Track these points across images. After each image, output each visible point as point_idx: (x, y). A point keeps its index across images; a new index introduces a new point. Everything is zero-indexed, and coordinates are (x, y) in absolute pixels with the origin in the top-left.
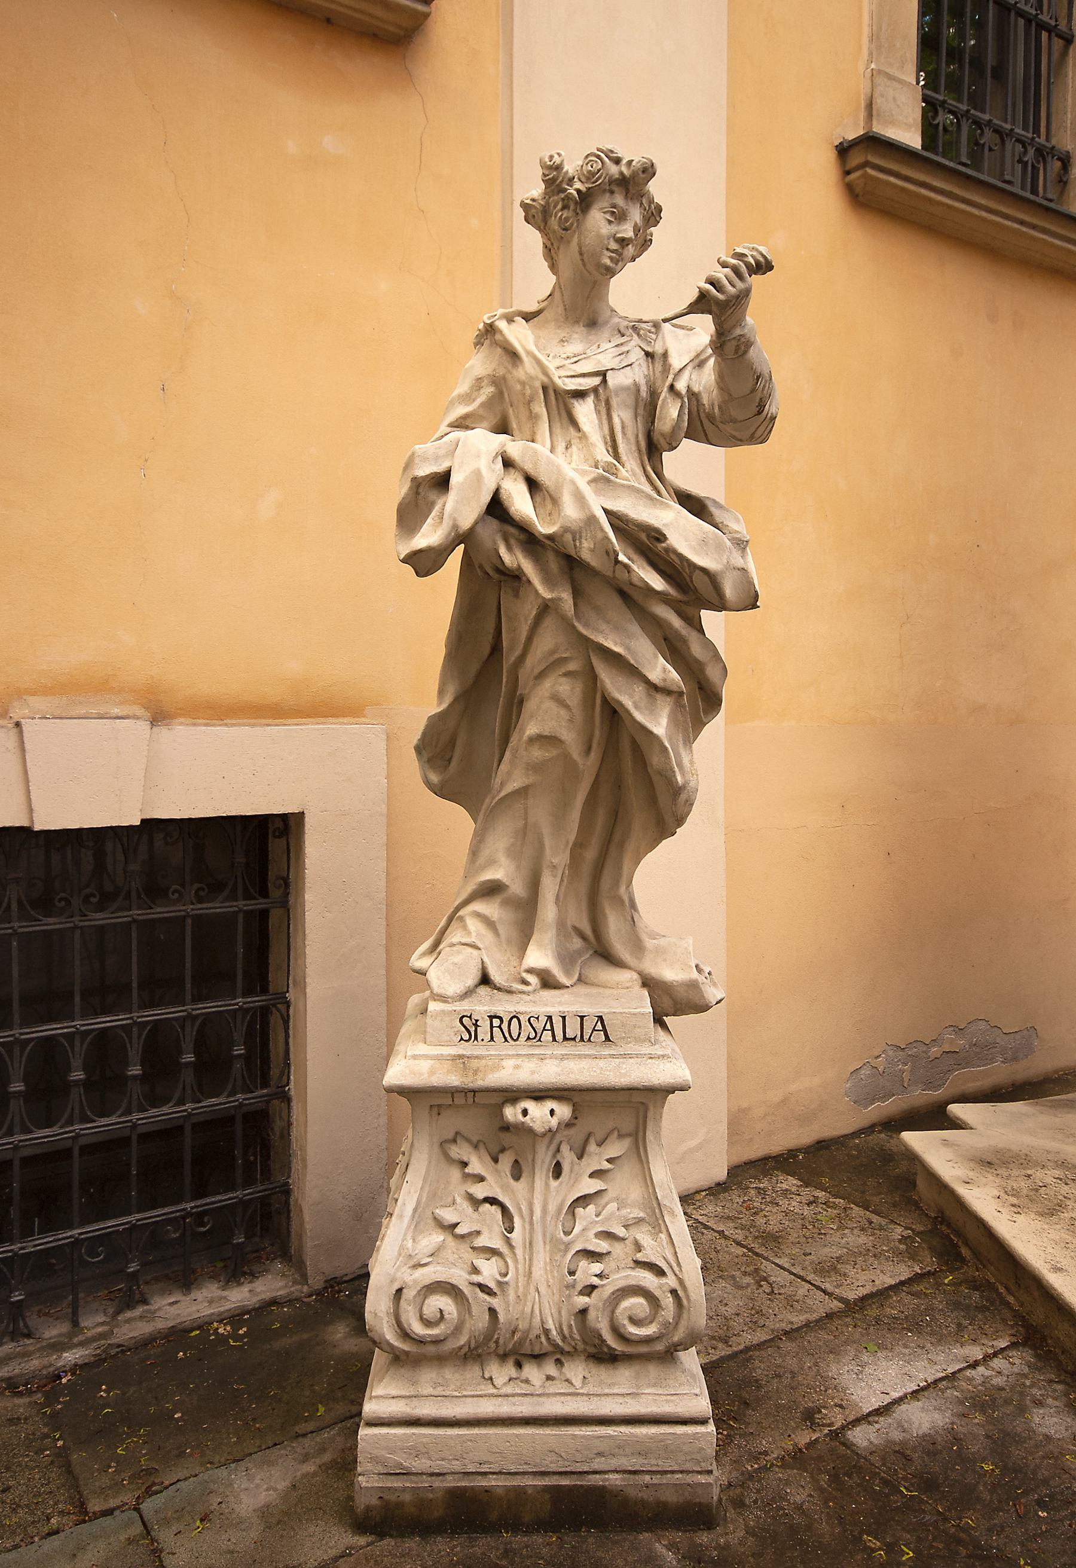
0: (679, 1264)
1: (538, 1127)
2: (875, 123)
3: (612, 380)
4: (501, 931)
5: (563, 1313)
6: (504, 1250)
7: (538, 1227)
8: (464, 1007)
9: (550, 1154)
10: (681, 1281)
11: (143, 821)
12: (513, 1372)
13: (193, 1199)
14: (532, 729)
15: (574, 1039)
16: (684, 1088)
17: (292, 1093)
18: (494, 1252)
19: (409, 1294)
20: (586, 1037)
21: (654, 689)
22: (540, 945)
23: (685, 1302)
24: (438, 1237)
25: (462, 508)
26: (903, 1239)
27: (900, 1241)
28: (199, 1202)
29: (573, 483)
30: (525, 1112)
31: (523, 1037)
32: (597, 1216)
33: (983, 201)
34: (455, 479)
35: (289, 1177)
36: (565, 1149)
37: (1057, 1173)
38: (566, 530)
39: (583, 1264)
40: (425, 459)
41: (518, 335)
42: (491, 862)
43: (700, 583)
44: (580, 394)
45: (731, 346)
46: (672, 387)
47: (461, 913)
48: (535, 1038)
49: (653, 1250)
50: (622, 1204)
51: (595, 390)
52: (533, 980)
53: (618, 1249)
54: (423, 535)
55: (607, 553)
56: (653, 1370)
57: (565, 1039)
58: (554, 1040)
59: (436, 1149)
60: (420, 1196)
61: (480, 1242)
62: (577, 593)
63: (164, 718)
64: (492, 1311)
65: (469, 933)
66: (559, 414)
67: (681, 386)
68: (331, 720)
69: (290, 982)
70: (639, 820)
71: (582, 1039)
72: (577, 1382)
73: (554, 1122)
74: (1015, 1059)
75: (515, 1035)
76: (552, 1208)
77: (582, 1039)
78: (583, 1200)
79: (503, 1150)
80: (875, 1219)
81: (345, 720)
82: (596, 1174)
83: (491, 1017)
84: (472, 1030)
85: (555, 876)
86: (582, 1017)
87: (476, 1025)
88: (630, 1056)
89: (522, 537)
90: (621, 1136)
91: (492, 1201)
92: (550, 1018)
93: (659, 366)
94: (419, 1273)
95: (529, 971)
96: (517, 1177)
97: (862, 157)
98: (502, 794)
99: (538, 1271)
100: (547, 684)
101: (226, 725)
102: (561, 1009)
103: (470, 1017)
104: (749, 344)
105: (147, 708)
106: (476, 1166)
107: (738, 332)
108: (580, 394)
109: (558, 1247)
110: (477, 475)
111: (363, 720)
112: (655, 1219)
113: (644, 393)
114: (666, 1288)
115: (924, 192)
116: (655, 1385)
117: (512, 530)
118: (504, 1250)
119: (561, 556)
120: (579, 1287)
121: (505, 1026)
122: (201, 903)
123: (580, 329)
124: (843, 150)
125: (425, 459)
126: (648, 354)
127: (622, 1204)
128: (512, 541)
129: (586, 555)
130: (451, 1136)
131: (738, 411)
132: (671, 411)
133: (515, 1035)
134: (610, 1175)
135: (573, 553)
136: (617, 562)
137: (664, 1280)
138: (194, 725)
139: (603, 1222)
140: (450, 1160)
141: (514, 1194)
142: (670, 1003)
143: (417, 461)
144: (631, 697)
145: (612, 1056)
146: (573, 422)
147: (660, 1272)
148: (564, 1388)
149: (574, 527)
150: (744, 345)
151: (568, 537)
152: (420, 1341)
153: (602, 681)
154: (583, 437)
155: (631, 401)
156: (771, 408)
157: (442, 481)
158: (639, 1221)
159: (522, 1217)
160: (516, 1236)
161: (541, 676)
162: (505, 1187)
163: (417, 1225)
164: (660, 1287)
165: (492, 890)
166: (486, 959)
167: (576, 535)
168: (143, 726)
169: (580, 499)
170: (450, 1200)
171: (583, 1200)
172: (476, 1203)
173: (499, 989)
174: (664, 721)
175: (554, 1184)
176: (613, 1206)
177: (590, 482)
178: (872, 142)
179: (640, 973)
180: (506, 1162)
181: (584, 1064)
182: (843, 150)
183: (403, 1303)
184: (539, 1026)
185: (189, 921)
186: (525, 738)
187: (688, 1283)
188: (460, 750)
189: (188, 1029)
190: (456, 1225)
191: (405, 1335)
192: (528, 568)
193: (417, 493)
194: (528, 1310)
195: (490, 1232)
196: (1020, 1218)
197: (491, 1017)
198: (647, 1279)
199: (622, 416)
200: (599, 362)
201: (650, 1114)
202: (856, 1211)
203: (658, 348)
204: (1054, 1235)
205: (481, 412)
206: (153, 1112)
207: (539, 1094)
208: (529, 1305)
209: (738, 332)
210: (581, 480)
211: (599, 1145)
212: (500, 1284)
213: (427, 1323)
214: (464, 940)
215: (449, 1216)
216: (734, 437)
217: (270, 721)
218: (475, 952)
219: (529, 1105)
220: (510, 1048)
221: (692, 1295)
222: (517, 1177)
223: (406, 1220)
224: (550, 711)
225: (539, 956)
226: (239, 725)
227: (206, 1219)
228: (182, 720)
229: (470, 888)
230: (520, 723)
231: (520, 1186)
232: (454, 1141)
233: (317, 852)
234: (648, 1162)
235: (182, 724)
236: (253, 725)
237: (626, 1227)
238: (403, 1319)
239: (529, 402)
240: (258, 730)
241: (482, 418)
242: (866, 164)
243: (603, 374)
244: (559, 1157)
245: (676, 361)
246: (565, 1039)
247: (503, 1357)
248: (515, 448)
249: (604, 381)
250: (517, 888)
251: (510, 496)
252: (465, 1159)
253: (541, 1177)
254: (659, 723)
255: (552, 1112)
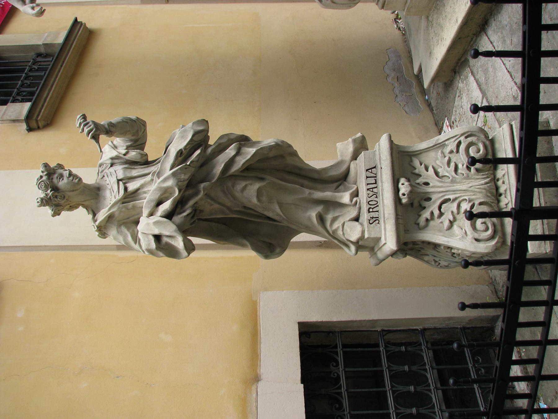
0: (456, 136)
1: (409, 189)
2: (21, 119)
3: (121, 176)
4: (337, 215)
5: (478, 177)
6: (457, 201)
7: (448, 189)
8: (366, 223)
9: (420, 187)
10: (462, 135)
11: (302, 383)
12: (503, 196)
13: (468, 364)
14: (255, 200)
15: (376, 180)
16: (390, 137)
17: (421, 327)
18: (459, 206)
19: (477, 236)
20: (375, 175)
21: (238, 153)
22: (341, 197)
23: (469, 133)
24: (455, 227)
25: (168, 229)
26: (463, 82)
27: (463, 83)
28: (469, 362)
29: (159, 183)
30: (404, 195)
31: (376, 199)
32: (441, 167)
33: (53, 79)
34: (157, 232)
35: (458, 328)
36: (418, 181)
37: (430, 28)
38: (177, 185)
39: (459, 171)
40: (149, 245)
41: (102, 216)
42: (310, 219)
43: (198, 138)
44: (126, 189)
45: (110, 130)
46: (125, 155)
47: (331, 232)
48: (376, 195)
49: (452, 146)
50: (437, 159)
51: (124, 184)
52: (355, 199)
53: (454, 160)
54: (179, 245)
55: (186, 168)
56: (497, 146)
57: (376, 183)
58: (376, 187)
59: (421, 231)
60: (441, 235)
61: (455, 211)
62: (202, 181)
63: (258, 377)
64: (481, 204)
65: (338, 227)
66: (133, 197)
67: (124, 152)
68: (258, 313)
69: (373, 329)
70: (289, 160)
71: (376, 177)
72: (503, 172)
73: (406, 183)
74: (399, 56)
75: (376, 203)
76: (440, 184)
77: (376, 177)
78: (437, 173)
79: (420, 205)
80: (457, 95)
81: (258, 308)
82: (427, 169)
83: (369, 212)
84: (374, 219)
85: (313, 193)
86: (367, 177)
87: (373, 218)
88: (380, 157)
89: (180, 206)
90: (412, 161)
91: (440, 208)
92: (368, 189)
93: (116, 161)
94: (468, 233)
95: (351, 201)
96: (429, 199)
97: (33, 123)
98: (281, 213)
99: (464, 187)
100: (237, 194)
101: (260, 354)
102: (364, 185)
103: (370, 220)
104: (111, 123)
105: (253, 384)
106: (426, 214)
107: (106, 126)
108: (126, 189)
109: (453, 181)
110: (156, 223)
111: (258, 301)
112: (441, 145)
113: (126, 166)
114: (465, 140)
115: (48, 100)
116: (501, 144)
117: (178, 210)
118: (457, 201)
119: (189, 187)
120: (468, 172)
121: (372, 207)
122: (339, 365)
123: (100, 192)
124: (30, 129)
125: (149, 245)
126: (112, 166)
127: (437, 159)
128: (182, 211)
129: (187, 177)
130: (416, 226)
131: (134, 131)
132: (133, 154)
133: (376, 203)
134: (427, 164)
135: (186, 183)
136: (189, 165)
137: (462, 141)
138: (260, 366)
139: (444, 165)
140: (426, 226)
141: (437, 199)
142: (361, 146)
143: (149, 248)
144: (241, 160)
145: (380, 164)
146: (136, 191)
147: (459, 143)
148: (506, 177)
149: (176, 181)
150: (111, 124)
151: (180, 183)
152: (495, 232)
153: (235, 171)
154: (142, 186)
155: (129, 170)
156: (133, 117)
157: (158, 238)
158: (442, 153)
159: (444, 196)
160: (452, 197)
161: (234, 197)
162: (434, 202)
163: (451, 236)
164: (464, 142)
165: (321, 219)
166: (348, 219)
167: (179, 181)
168: (261, 384)
169: (165, 180)
170: (441, 224)
171: (437, 173)
172: (441, 214)
173: (359, 213)
174: (251, 149)
175: (431, 185)
176: (438, 162)
177: (159, 179)
178: (29, 118)
179: (351, 161)
180: (426, 204)
181: (383, 173)
182: (30, 129)
183: (480, 238)
184: (371, 193)
185: (347, 369)
186: (258, 204)
187: (462, 132)
188: (268, 236)
189: (394, 369)
190: (450, 221)
191: (492, 238)
192: (191, 203)
193: (162, 248)
194: (478, 190)
195: (451, 207)
196: (445, 37)
197: (369, 212)
198: (462, 147)
199: (135, 173)
200: (114, 182)
201: (402, 150)
202: (456, 103)
203: (109, 162)
204: (448, 25)
205: (131, 231)
206: (430, 381)
207: (396, 190)
208: (476, 190)
209: (106, 126)
210: (159, 182)
211: (415, 169)
212: (470, 201)
213: (487, 229)
214: (341, 229)
215: (446, 223)
216: (144, 132)
217: (259, 337)
218: (346, 224)
219: (401, 193)
220: (380, 204)
221: (466, 130)
222: (429, 199)
223: (449, 240)
224: (250, 192)
225: (346, 198)
226: (260, 347)
227: (476, 359)
228: (258, 370)
229: (320, 229)
230: (253, 208)
231: (434, 197)
232: (418, 224)
233: (315, 316)
234: (420, 150)
235: (260, 371)
236: (260, 343)
237: (445, 157)
238: (486, 238)
239: (128, 209)
240: (262, 340)
241: (133, 231)
242: (37, 121)
243: (119, 181)
244: (421, 184)
245: (114, 153)
246: (376, 183)
247: (499, 201)
248: (145, 212)
249: (121, 180)
250: (320, 209)
251: (164, 211)
252: (425, 219)
253: (429, 189)
254: (252, 151)
255: (403, 184)
